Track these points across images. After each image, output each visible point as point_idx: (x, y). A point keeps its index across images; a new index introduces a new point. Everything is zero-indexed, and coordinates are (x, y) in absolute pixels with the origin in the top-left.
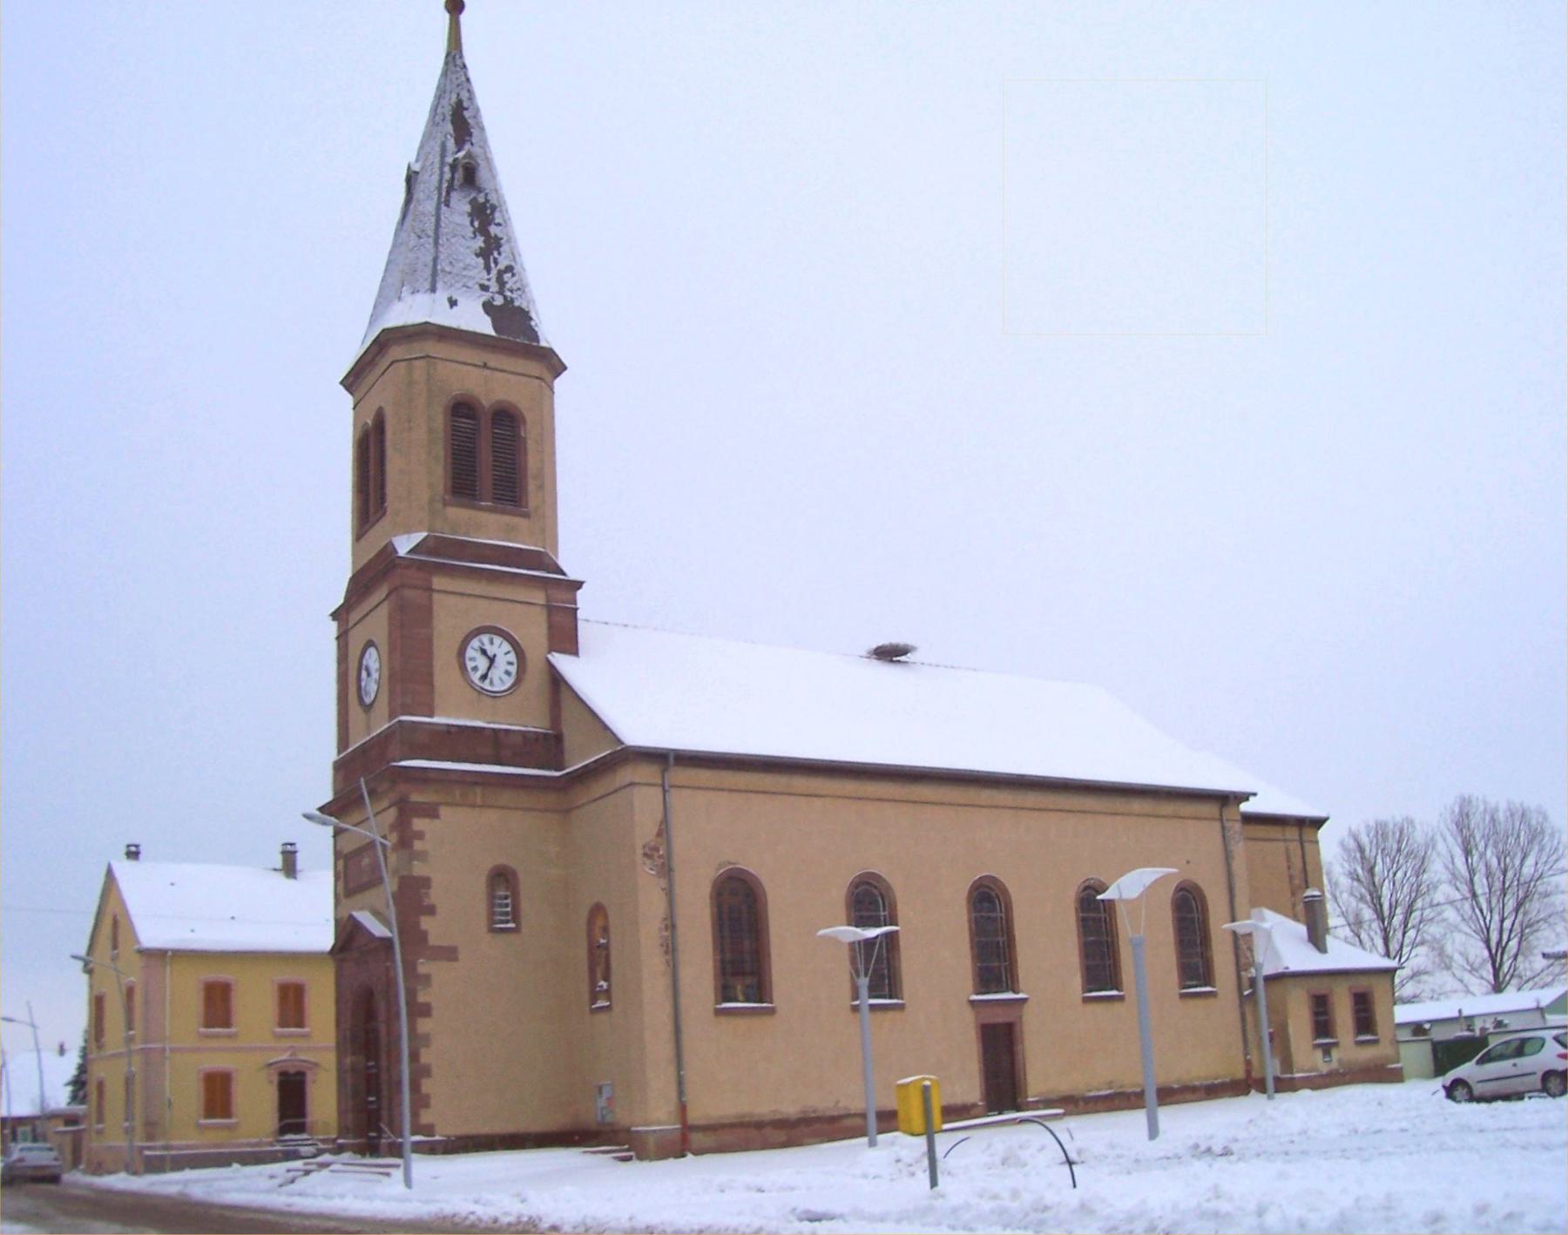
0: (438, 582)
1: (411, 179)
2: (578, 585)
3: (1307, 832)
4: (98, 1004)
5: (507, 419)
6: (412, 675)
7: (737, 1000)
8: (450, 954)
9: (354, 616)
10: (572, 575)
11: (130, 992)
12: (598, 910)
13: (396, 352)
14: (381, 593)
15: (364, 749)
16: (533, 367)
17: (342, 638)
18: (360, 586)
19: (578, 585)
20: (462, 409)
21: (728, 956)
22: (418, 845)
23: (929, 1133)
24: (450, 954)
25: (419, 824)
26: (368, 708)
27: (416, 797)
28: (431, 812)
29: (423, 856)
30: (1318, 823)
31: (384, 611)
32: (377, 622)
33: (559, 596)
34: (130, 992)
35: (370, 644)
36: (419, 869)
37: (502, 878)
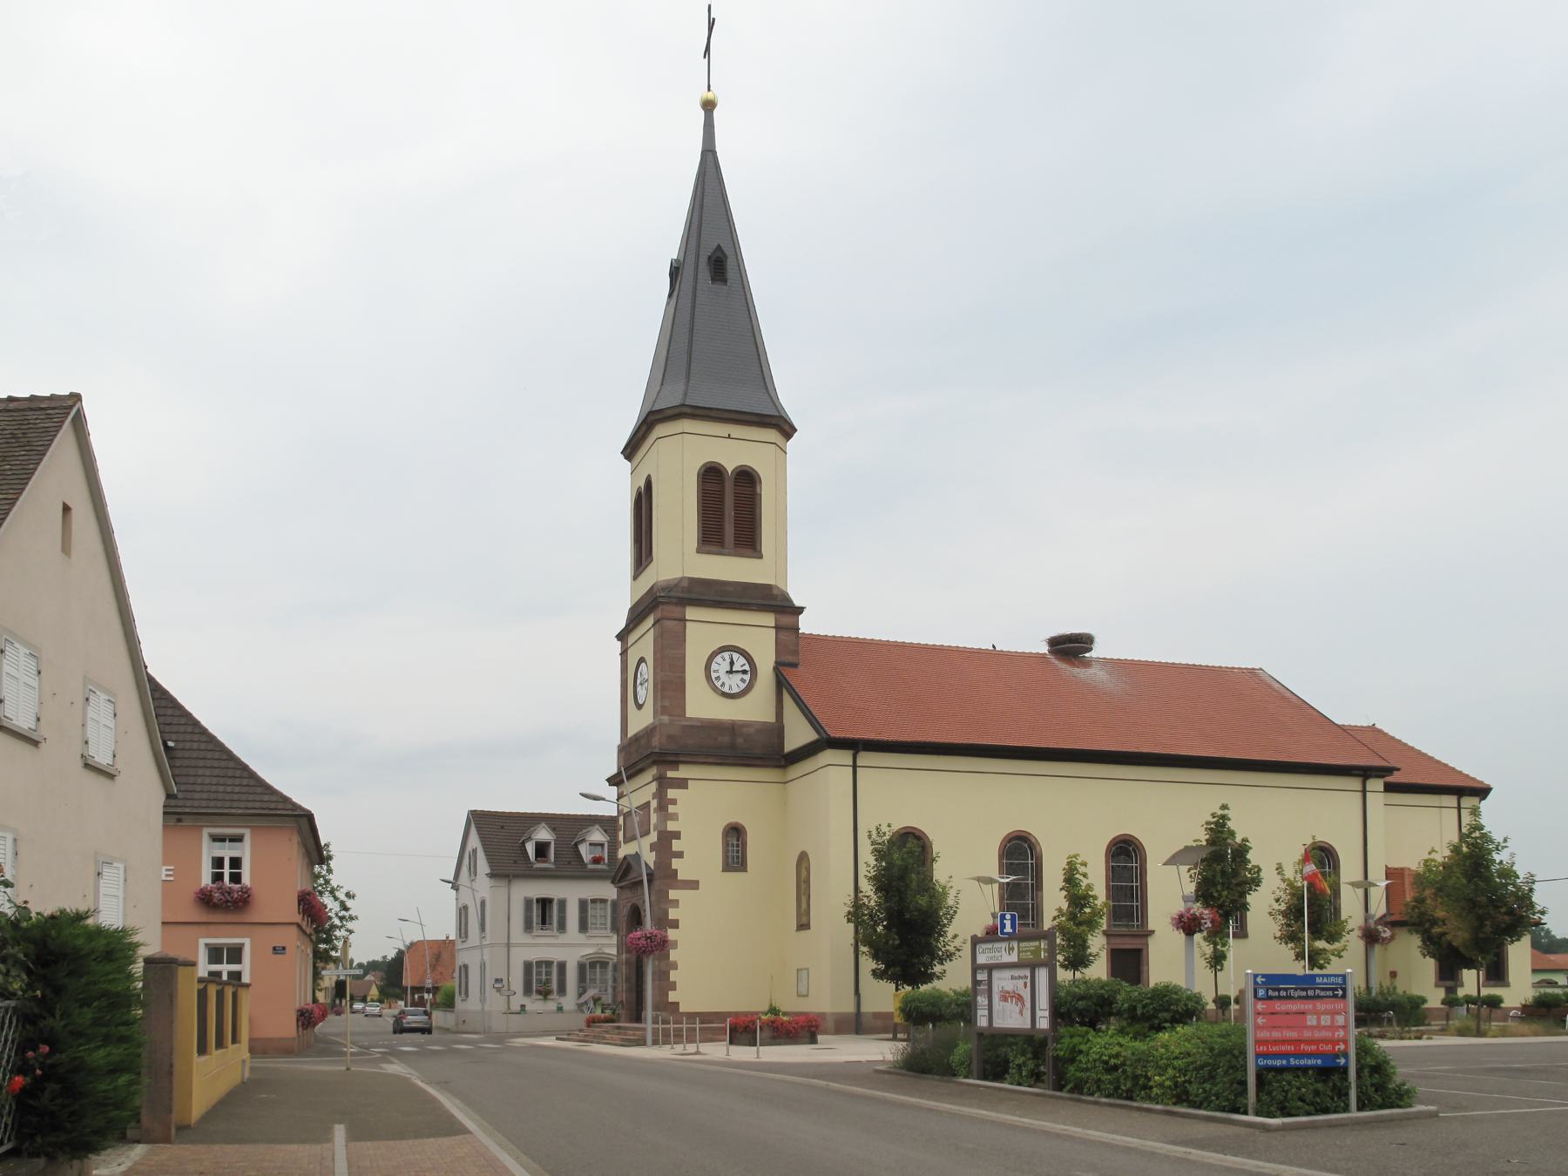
0: (691, 613)
1: (675, 272)
2: (800, 610)
3: (1468, 802)
4: (463, 912)
5: (747, 478)
6: (671, 685)
7: (1246, 1113)
8: (693, 885)
9: (632, 638)
10: (797, 603)
11: (483, 903)
12: (803, 858)
13: (660, 430)
14: (650, 621)
15: (637, 738)
16: (772, 435)
17: (624, 653)
18: (637, 616)
19: (800, 610)
20: (711, 475)
21: (641, 720)
22: (671, 809)
23: (858, 1013)
24: (693, 885)
25: (672, 793)
26: (639, 707)
27: (670, 774)
28: (682, 784)
29: (674, 817)
30: (1482, 792)
31: (650, 636)
32: (644, 643)
33: (786, 620)
34: (483, 903)
35: (642, 660)
36: (671, 826)
37: (735, 833)
